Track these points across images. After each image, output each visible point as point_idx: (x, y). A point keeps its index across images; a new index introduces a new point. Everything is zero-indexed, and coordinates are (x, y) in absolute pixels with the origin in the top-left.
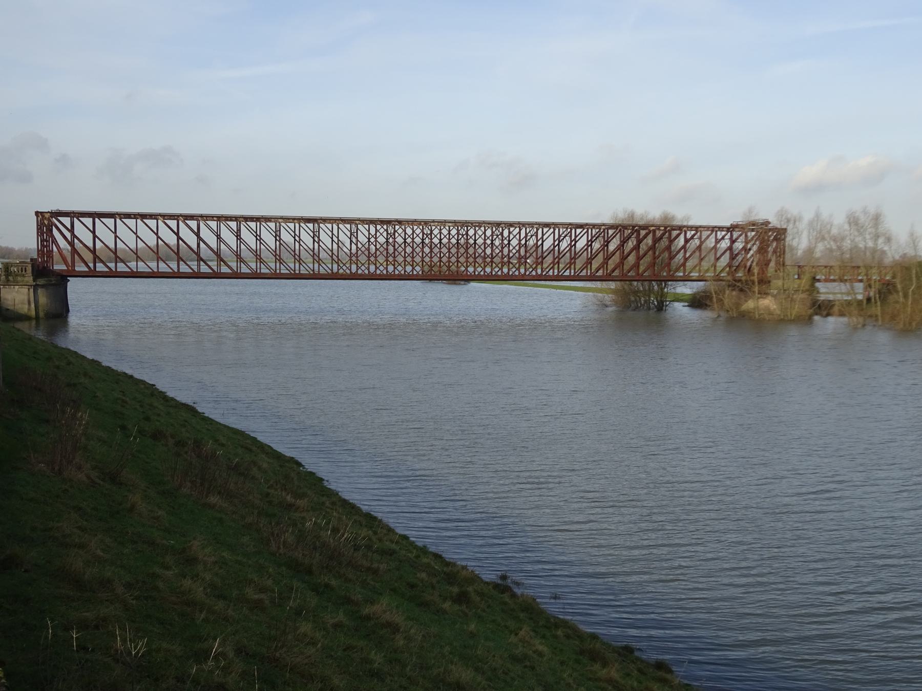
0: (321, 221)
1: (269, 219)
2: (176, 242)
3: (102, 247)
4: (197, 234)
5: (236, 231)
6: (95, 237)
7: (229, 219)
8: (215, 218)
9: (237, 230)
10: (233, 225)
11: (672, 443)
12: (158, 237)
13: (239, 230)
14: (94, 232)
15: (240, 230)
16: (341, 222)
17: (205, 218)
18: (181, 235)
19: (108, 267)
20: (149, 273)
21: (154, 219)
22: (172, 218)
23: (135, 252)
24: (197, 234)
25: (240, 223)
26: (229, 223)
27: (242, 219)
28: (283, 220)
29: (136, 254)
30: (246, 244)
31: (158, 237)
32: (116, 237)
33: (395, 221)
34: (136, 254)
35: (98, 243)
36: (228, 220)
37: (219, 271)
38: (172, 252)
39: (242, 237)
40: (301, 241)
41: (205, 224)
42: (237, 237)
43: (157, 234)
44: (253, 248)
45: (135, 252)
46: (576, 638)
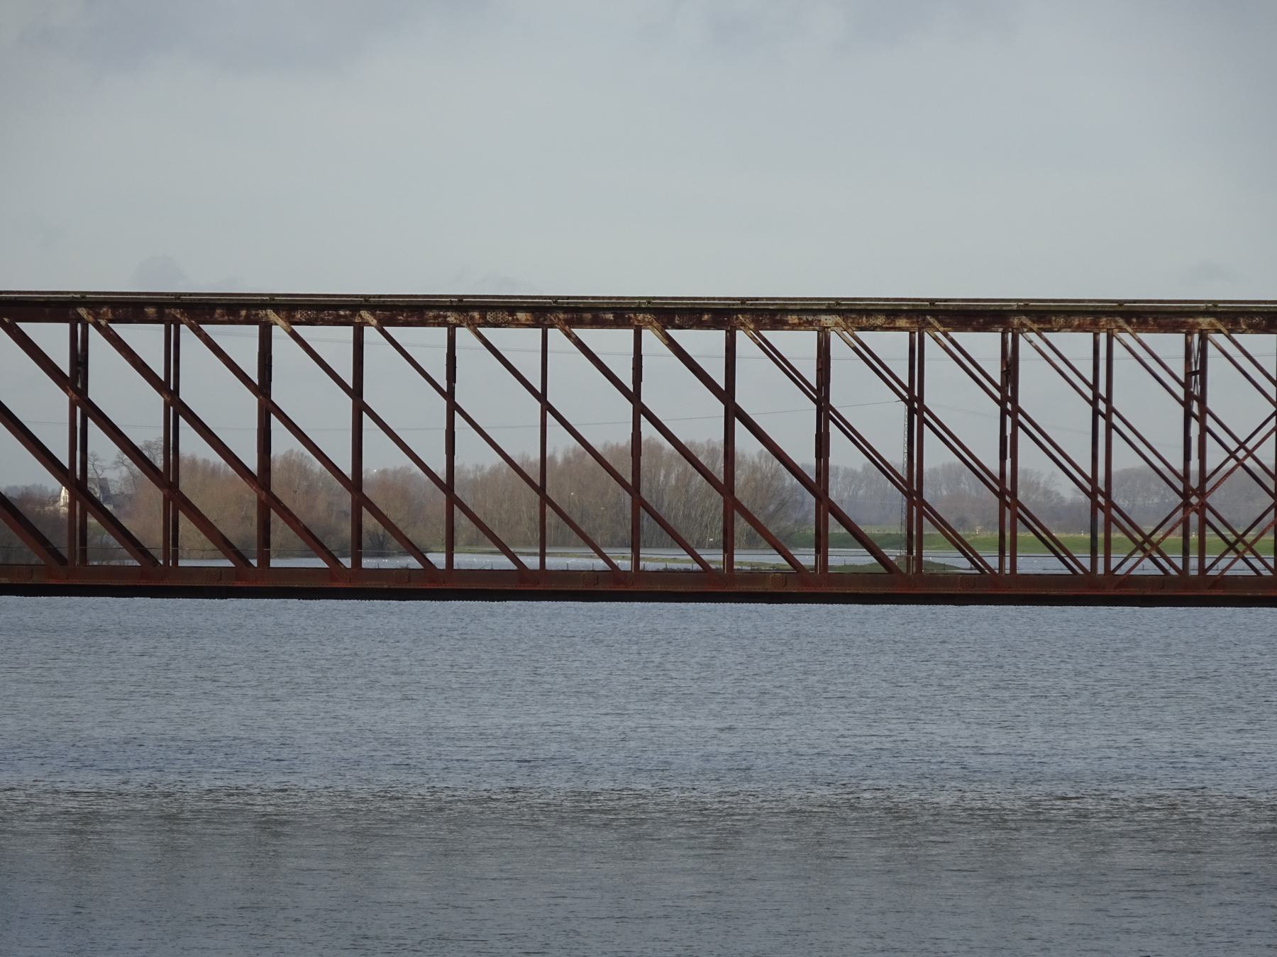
0: (1025, 319)
1: (773, 313)
2: (719, 436)
3: (495, 471)
4: (167, 387)
5: (999, 382)
6: (268, 409)
7: (588, 316)
8: (521, 316)
9: (1188, 374)
10: (1170, 346)
11: (1021, 757)
12: (640, 411)
13: (80, 359)
14: (262, 388)
15: (1203, 372)
16: (1121, 322)
17: (476, 315)
18: (629, 406)
19: (697, 559)
20: (965, 579)
21: (248, 321)
22: (325, 315)
23: (537, 481)
24: (167, 387)
25: (1204, 339)
26: (963, 338)
27: (649, 317)
28: (838, 319)
29: (541, 490)
30: (1140, 443)
31: (640, 411)
32: (360, 408)
33: (1018, 312)
34: (541, 490)
35: (282, 441)
36: (582, 324)
37: (1101, 570)
38: (790, 480)
39: (1021, 404)
40: (1208, 417)
41: (855, 349)
42: (1001, 403)
43: (634, 396)
44: (1175, 467)
45: (537, 481)
46: (672, 870)
